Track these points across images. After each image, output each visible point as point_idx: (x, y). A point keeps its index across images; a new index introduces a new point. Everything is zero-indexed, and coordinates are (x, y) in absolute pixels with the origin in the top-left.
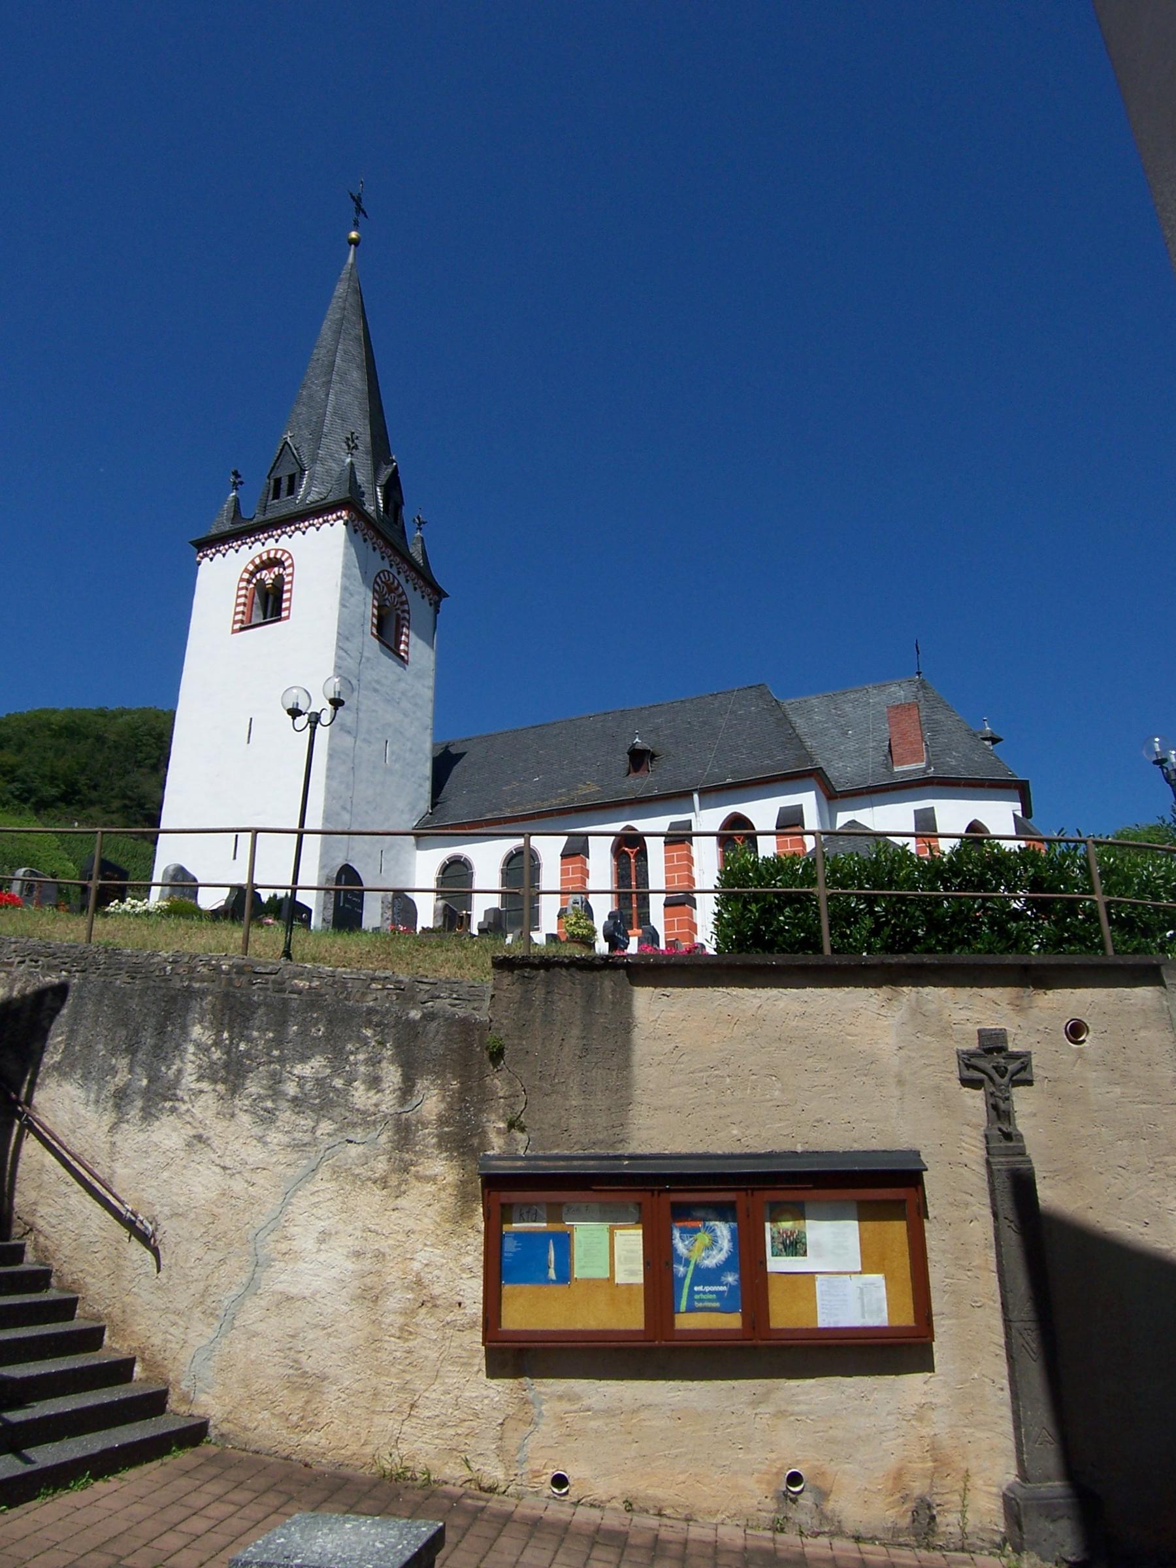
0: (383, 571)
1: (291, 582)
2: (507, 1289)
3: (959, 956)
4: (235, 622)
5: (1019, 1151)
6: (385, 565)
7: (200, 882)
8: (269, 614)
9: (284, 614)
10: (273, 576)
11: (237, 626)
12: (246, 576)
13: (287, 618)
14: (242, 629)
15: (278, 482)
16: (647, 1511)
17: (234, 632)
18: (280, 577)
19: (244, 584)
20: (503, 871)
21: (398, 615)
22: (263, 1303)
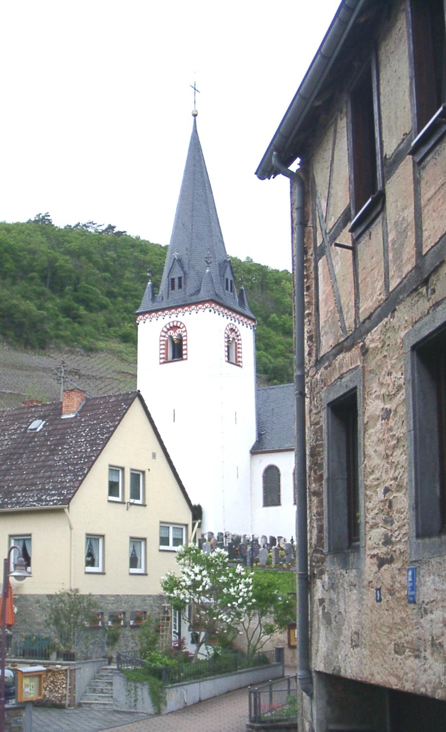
0: (230, 324)
1: (186, 340)
2: (285, 669)
3: (419, 476)
4: (161, 359)
5: (133, 540)
6: (229, 321)
7: (194, 109)
8: (176, 356)
9: (184, 357)
10: (176, 335)
11: (162, 361)
12: (165, 330)
13: (186, 359)
14: (164, 363)
15: (180, 287)
16: (272, 679)
17: (161, 363)
18: (180, 335)
19: (163, 334)
20: (263, 476)
21: (236, 343)
22: (78, 263)
